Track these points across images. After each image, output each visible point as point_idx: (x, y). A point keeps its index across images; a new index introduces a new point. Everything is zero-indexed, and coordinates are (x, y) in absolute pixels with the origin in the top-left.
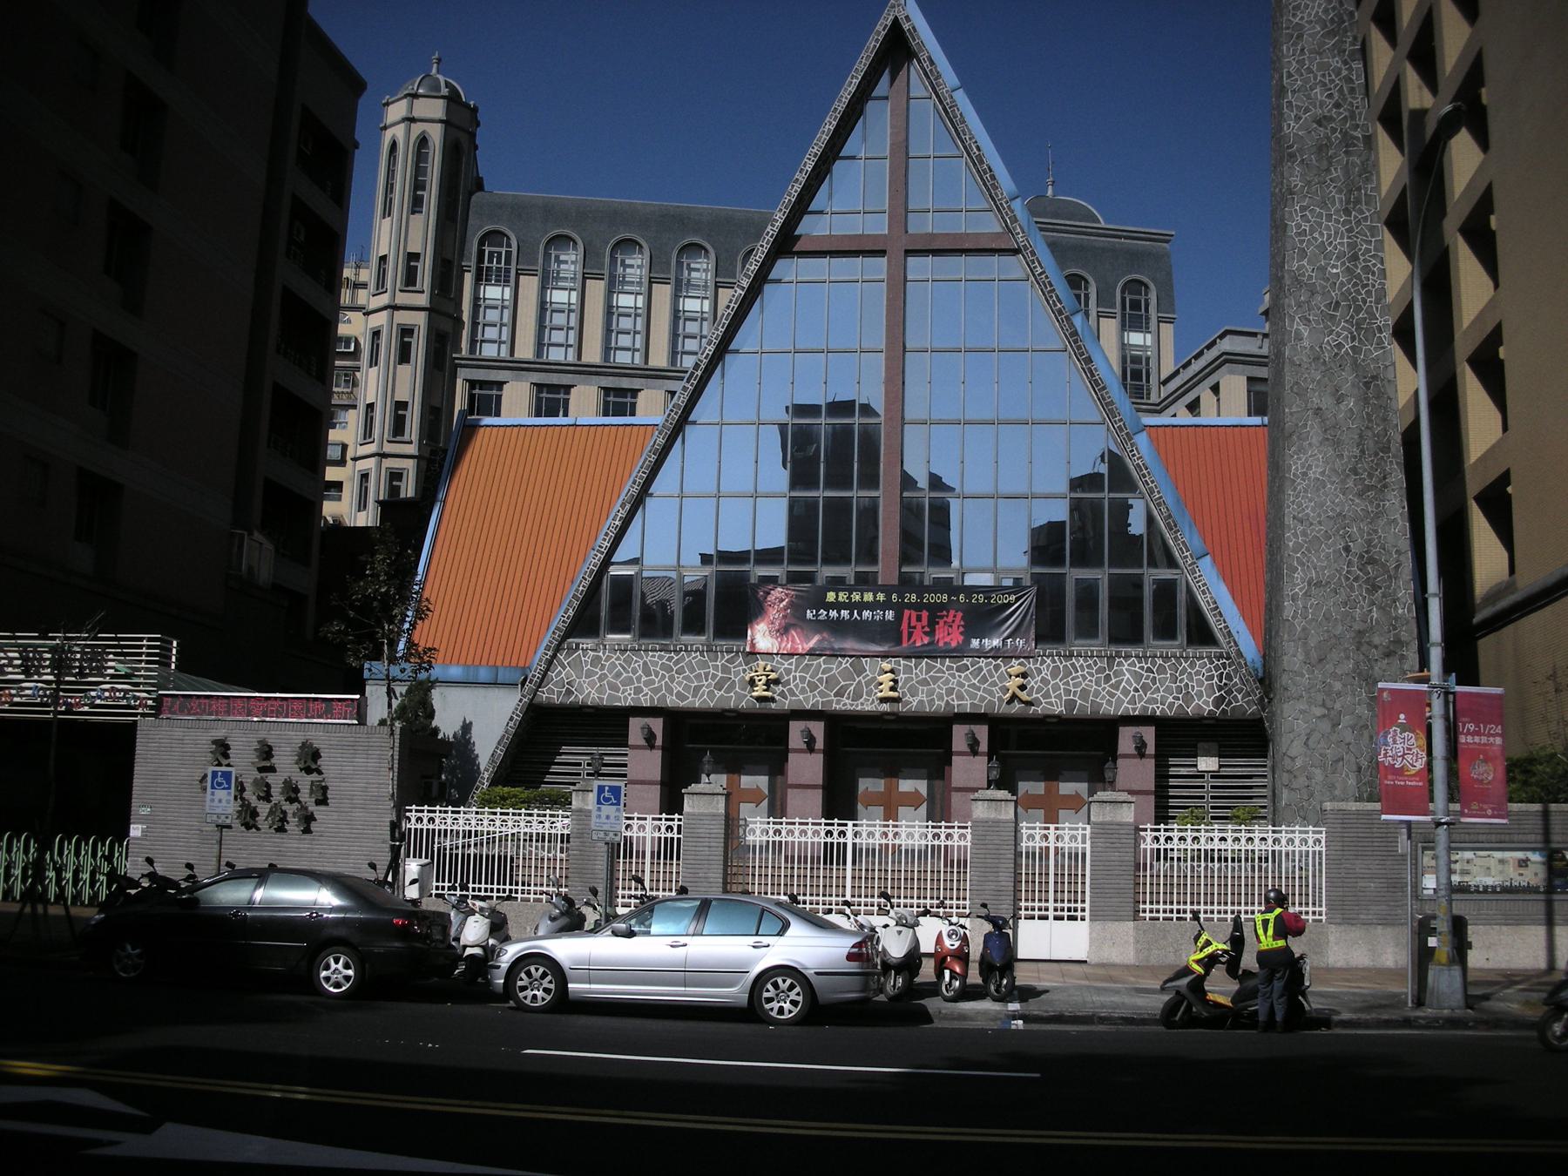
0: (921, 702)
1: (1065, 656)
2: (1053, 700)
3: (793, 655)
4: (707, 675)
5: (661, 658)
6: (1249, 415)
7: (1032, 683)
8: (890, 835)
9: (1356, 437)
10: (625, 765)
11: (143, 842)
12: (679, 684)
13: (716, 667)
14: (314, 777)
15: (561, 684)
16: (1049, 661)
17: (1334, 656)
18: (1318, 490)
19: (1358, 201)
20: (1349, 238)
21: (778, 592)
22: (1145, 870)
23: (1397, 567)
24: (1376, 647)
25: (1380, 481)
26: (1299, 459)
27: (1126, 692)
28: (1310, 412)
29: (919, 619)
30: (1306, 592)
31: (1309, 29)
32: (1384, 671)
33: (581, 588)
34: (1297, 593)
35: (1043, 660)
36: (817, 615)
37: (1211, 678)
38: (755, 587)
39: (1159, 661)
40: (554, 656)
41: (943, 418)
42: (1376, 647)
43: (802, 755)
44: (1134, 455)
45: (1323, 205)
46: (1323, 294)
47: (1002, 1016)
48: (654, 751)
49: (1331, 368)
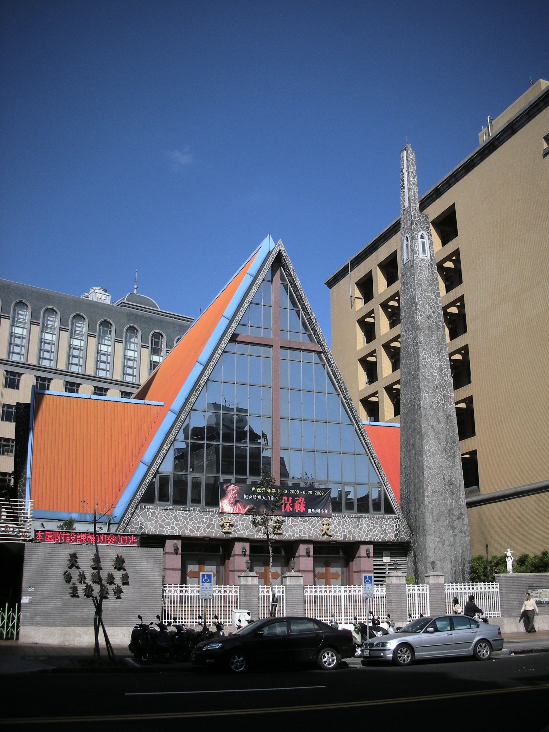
0: (290, 535)
1: (343, 517)
2: (339, 534)
3: (239, 514)
4: (203, 522)
5: (183, 513)
6: (207, 404)
7: (331, 528)
8: (184, 591)
9: (445, 437)
10: (374, 565)
11: (30, 605)
12: (191, 525)
13: (206, 519)
14: (122, 572)
15: (138, 524)
16: (337, 519)
17: (442, 518)
18: (434, 456)
19: (441, 350)
20: (439, 362)
21: (232, 487)
22: (308, 603)
23: (460, 486)
24: (455, 516)
25: (453, 454)
26: (427, 444)
27: (364, 532)
28: (430, 427)
29: (288, 500)
30: (432, 495)
31: (423, 282)
32: (458, 524)
33: (148, 480)
34: (429, 495)
35: (334, 518)
36: (248, 497)
37: (393, 526)
38: (221, 484)
39: (376, 520)
40: (134, 511)
41: (295, 417)
42: (455, 516)
43: (173, 555)
44: (366, 438)
45: (431, 350)
46: (432, 383)
47: (508, 653)
48: (178, 555)
49: (436, 411)
